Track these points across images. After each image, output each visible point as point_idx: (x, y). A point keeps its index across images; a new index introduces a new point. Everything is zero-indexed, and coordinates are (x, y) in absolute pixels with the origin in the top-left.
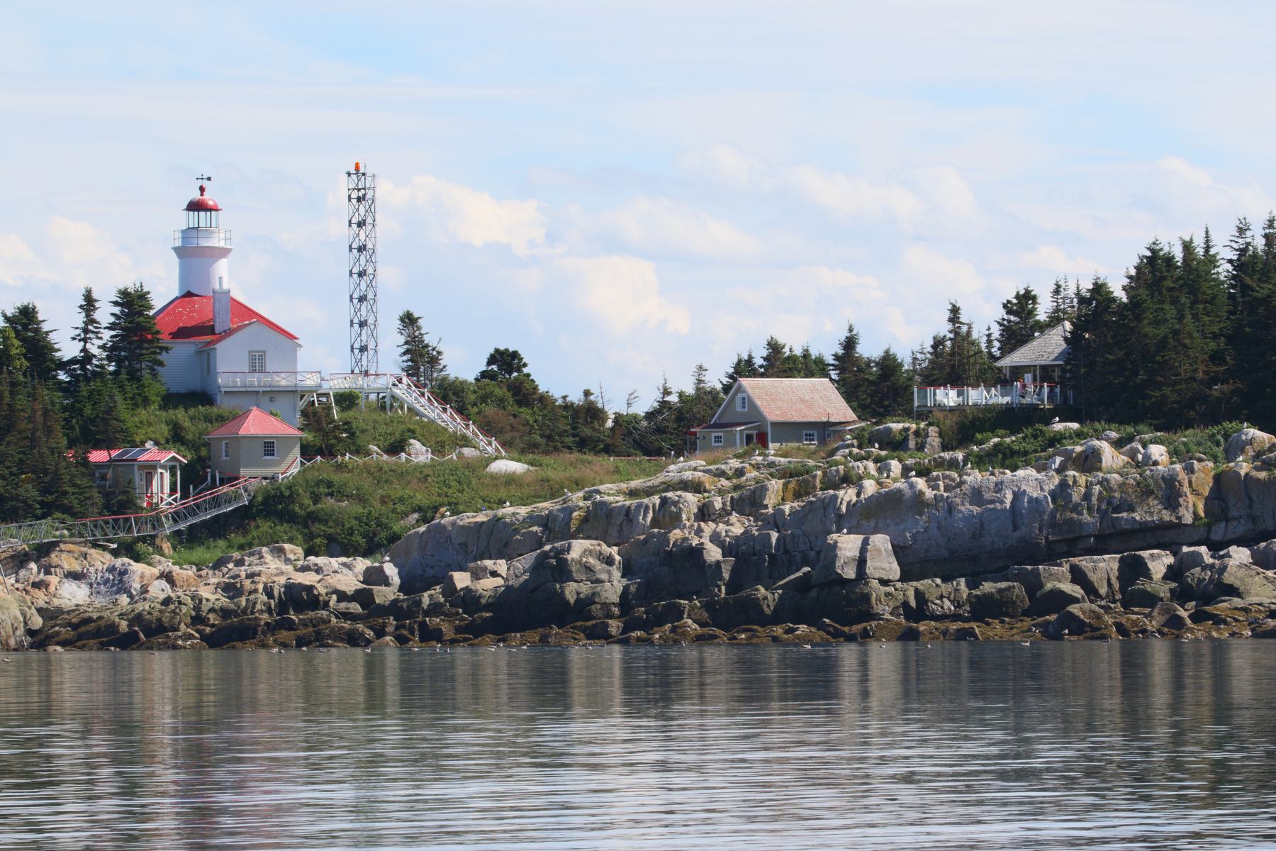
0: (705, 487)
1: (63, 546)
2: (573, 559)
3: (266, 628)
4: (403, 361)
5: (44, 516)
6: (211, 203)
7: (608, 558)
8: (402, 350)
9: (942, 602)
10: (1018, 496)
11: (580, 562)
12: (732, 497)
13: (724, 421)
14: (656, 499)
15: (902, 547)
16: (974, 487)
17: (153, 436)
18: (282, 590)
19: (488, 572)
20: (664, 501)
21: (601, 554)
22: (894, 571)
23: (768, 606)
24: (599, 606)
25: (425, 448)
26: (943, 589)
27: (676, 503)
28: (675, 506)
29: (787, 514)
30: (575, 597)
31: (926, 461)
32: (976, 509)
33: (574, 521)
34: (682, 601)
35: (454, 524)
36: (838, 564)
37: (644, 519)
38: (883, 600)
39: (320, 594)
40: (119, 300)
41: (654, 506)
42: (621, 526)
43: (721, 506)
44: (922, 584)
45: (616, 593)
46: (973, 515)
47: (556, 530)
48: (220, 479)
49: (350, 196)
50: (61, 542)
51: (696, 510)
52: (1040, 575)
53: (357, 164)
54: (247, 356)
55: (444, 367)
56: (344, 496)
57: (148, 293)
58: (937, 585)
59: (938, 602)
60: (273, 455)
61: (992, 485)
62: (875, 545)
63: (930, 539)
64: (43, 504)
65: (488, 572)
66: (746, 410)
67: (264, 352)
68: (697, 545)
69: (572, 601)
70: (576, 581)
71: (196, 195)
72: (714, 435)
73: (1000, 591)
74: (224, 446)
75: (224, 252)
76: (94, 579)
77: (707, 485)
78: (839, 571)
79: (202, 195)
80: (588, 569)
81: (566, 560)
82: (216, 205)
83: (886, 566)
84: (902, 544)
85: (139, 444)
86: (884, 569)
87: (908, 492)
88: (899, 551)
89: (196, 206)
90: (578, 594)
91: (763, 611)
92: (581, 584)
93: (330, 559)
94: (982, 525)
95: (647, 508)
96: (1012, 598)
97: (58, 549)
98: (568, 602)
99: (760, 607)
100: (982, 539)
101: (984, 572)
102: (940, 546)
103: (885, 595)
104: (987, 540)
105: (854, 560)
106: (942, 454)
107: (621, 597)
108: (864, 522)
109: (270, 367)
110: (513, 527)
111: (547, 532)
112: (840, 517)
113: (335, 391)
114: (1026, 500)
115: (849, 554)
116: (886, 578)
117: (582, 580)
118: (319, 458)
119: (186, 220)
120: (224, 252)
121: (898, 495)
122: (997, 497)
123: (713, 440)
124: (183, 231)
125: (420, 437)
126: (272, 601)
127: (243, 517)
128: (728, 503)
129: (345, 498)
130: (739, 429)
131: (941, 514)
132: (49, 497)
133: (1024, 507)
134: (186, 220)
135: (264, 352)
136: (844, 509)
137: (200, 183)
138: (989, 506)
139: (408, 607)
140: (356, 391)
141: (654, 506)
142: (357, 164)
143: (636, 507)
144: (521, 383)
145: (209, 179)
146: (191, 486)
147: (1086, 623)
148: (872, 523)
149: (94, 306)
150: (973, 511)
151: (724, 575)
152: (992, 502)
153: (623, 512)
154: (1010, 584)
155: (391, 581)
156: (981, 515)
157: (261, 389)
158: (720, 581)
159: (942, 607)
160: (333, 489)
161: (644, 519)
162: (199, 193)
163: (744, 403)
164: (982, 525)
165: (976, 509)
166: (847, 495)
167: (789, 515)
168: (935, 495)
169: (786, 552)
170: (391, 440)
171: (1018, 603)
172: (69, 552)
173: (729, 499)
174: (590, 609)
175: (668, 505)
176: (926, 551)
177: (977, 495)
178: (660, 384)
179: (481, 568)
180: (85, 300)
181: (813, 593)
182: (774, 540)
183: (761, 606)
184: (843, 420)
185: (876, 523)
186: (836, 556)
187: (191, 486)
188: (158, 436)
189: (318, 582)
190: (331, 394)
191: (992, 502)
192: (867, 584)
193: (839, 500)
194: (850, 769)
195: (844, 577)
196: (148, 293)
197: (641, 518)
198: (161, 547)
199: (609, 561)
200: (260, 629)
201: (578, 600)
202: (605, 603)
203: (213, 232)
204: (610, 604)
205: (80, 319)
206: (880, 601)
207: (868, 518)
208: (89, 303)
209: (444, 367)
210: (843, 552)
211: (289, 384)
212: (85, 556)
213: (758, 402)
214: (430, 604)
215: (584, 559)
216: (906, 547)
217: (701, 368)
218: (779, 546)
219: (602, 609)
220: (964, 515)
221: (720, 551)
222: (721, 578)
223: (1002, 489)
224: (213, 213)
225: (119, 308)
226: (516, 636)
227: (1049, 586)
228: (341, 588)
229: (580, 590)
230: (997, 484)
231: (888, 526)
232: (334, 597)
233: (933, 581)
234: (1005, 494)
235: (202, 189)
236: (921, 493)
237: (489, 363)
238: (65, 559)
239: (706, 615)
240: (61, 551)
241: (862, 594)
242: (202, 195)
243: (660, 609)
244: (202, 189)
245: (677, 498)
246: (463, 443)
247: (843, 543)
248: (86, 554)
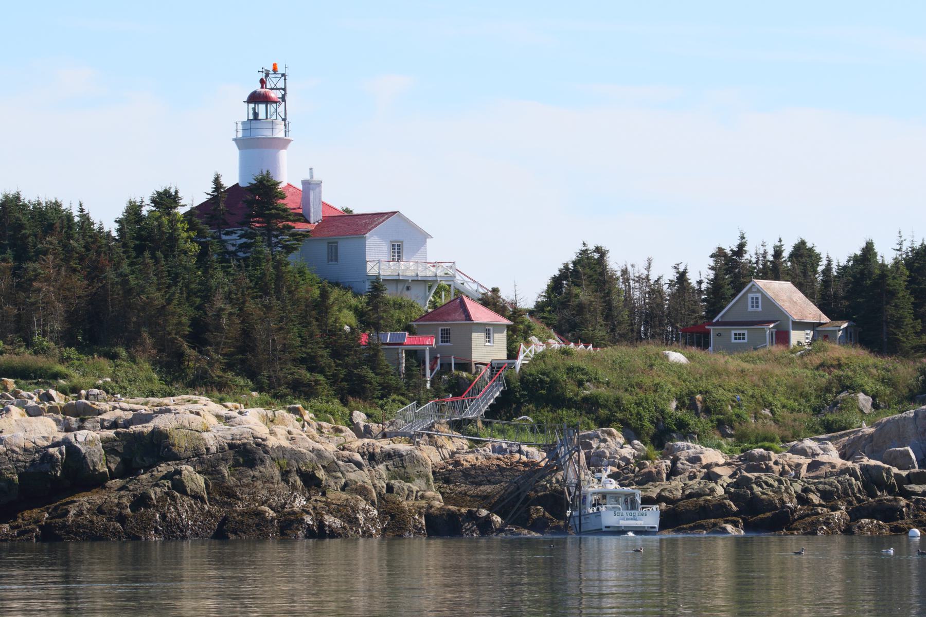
8: (579, 252)
13: (727, 319)
48: (455, 364)
53: (275, 65)
66: (760, 309)
71: (257, 87)
72: (733, 332)
74: (440, 332)
79: (262, 87)
89: (255, 98)
119: (243, 112)
123: (733, 336)
124: (243, 123)
129: (601, 385)
142: (275, 65)
162: (260, 85)
184: (766, 320)
194: (256, 594)
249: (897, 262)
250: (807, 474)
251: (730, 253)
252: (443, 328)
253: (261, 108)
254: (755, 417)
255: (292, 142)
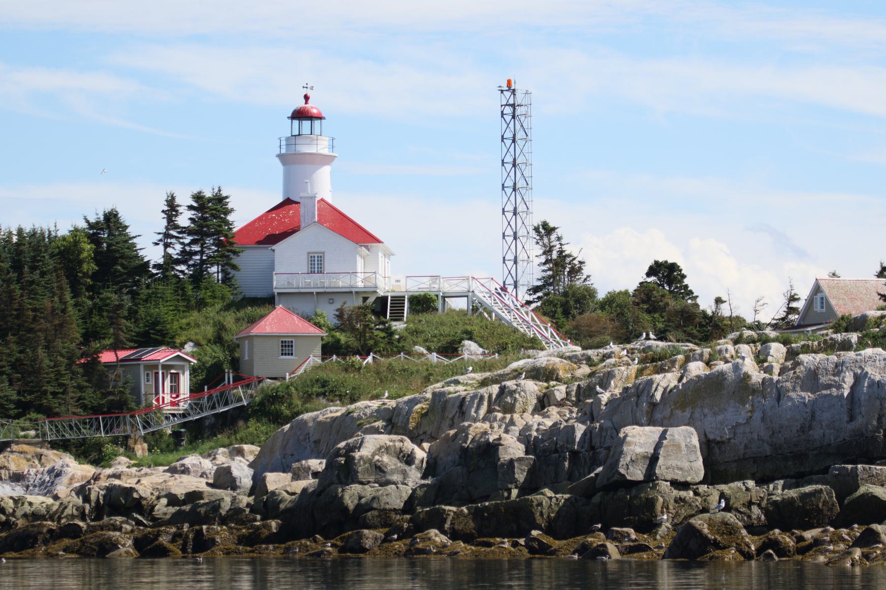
0: (558, 375)
1: (14, 447)
2: (361, 458)
3: (48, 536)
4: (543, 271)
5: (17, 417)
6: (315, 111)
7: (409, 456)
9: (750, 509)
10: (858, 379)
11: (370, 461)
12: (579, 385)
14: (495, 389)
15: (718, 442)
16: (810, 369)
17: (193, 337)
18: (102, 492)
19: (310, 473)
20: (502, 390)
21: (401, 451)
22: (696, 469)
23: (542, 514)
24: (376, 513)
25: (481, 350)
26: (754, 493)
27: (512, 393)
28: (511, 397)
29: (603, 403)
30: (356, 502)
31: (816, 343)
32: (808, 396)
33: (414, 415)
34: (447, 508)
35: (314, 419)
36: (622, 462)
37: (477, 412)
38: (671, 507)
39: (141, 498)
40: (195, 205)
41: (490, 396)
42: (452, 419)
43: (564, 395)
44: (730, 488)
45: (401, 497)
46: (804, 403)
47: (399, 424)
49: (502, 112)
50: (13, 442)
51: (535, 401)
52: (857, 476)
54: (306, 257)
55: (588, 276)
56: (336, 396)
57: (227, 197)
58: (747, 489)
59: (743, 509)
60: (292, 354)
61: (831, 366)
62: (673, 440)
63: (751, 433)
64: (19, 404)
65: (310, 473)
66: (824, 310)
67: (323, 253)
68: (494, 440)
69: (351, 507)
70: (362, 483)
73: (804, 496)
75: (327, 160)
76: (32, 482)
77: (561, 373)
78: (622, 471)
79: (306, 103)
80: (379, 469)
81: (354, 458)
82: (320, 113)
83: (686, 465)
84: (718, 439)
85: (178, 345)
86: (681, 469)
87: (731, 376)
88: (709, 447)
89: (300, 115)
90: (360, 498)
91: (534, 519)
92: (367, 487)
93: (202, 460)
94: (813, 416)
95: (482, 398)
96: (818, 506)
97: (9, 449)
98: (346, 509)
99: (532, 514)
100: (811, 432)
101: (811, 473)
102: (763, 441)
103: (676, 501)
104: (816, 434)
105: (645, 457)
106: (834, 336)
107: (406, 503)
108: (679, 412)
109: (328, 267)
110: (359, 422)
111: (390, 427)
112: (653, 405)
113: (411, 294)
114: (866, 385)
115: (639, 450)
116: (682, 480)
117: (369, 482)
118: (334, 357)
119: (288, 128)
120: (327, 160)
121: (720, 378)
122: (834, 380)
124: (287, 139)
125: (478, 339)
126: (87, 506)
127: (242, 414)
128: (573, 393)
129: (337, 398)
130: (809, 329)
131: (768, 402)
132: (29, 397)
133: (863, 393)
134: (288, 128)
135: (323, 253)
136: (658, 396)
137: (304, 92)
138: (824, 392)
139: (205, 513)
140: (430, 293)
141: (490, 396)
143: (471, 397)
144: (651, 291)
145: (312, 88)
146: (206, 387)
147: (709, 540)
148: (687, 414)
149: (177, 211)
150: (804, 398)
151: (516, 476)
152: (828, 387)
153: (457, 404)
154: (819, 487)
155: (238, 484)
156: (814, 402)
157: (315, 291)
158: (511, 483)
159: (749, 517)
160: (326, 388)
161: (477, 412)
162: (304, 101)
163: (822, 303)
164: (813, 416)
165: (808, 396)
166: (665, 380)
167: (606, 405)
168: (764, 379)
169: (592, 448)
170: (444, 341)
171: (825, 512)
172: (21, 453)
173: (575, 388)
174: (366, 516)
175: (505, 395)
176: (746, 447)
177: (812, 379)
178: (785, 288)
179: (304, 469)
180: (168, 205)
181: (596, 499)
182: (579, 435)
183: (533, 514)
185: (692, 413)
186: (621, 452)
187: (206, 387)
188: (199, 337)
189: (137, 483)
190: (406, 297)
191: (828, 387)
192: (654, 487)
193: (654, 386)
195: (629, 478)
196: (227, 197)
197: (473, 410)
198: (134, 448)
199: (409, 459)
200: (40, 537)
201: (358, 506)
202: (385, 510)
203: (313, 140)
204: (390, 510)
205: (161, 224)
206: (668, 508)
207: (683, 406)
208: (172, 209)
209: (588, 276)
210: (632, 447)
211: (345, 285)
212: (40, 457)
213: (833, 302)
214: (230, 509)
215: (377, 457)
216: (723, 443)
217: (834, 274)
218: (584, 442)
219: (379, 516)
220: (794, 403)
221: (522, 447)
222: (514, 481)
223: (842, 371)
224: (317, 123)
225: (193, 212)
226: (267, 549)
227: (862, 490)
228: (174, 491)
229: (363, 494)
230: (837, 365)
231: (705, 416)
232: (164, 501)
233: (744, 484)
234: (844, 377)
235: (306, 98)
236: (747, 377)
237: (648, 275)
238: (13, 460)
239: (472, 524)
240: (12, 452)
241: (647, 499)
242: (306, 103)
243: (421, 516)
244: (306, 98)
245: (515, 387)
246: (530, 345)
247: (634, 436)
248: (41, 455)
249: (645, 476)
250: (672, 501)
251: (100, 355)
252: (284, 340)
253: (306, 124)
254: (763, 397)
255: (336, 159)
